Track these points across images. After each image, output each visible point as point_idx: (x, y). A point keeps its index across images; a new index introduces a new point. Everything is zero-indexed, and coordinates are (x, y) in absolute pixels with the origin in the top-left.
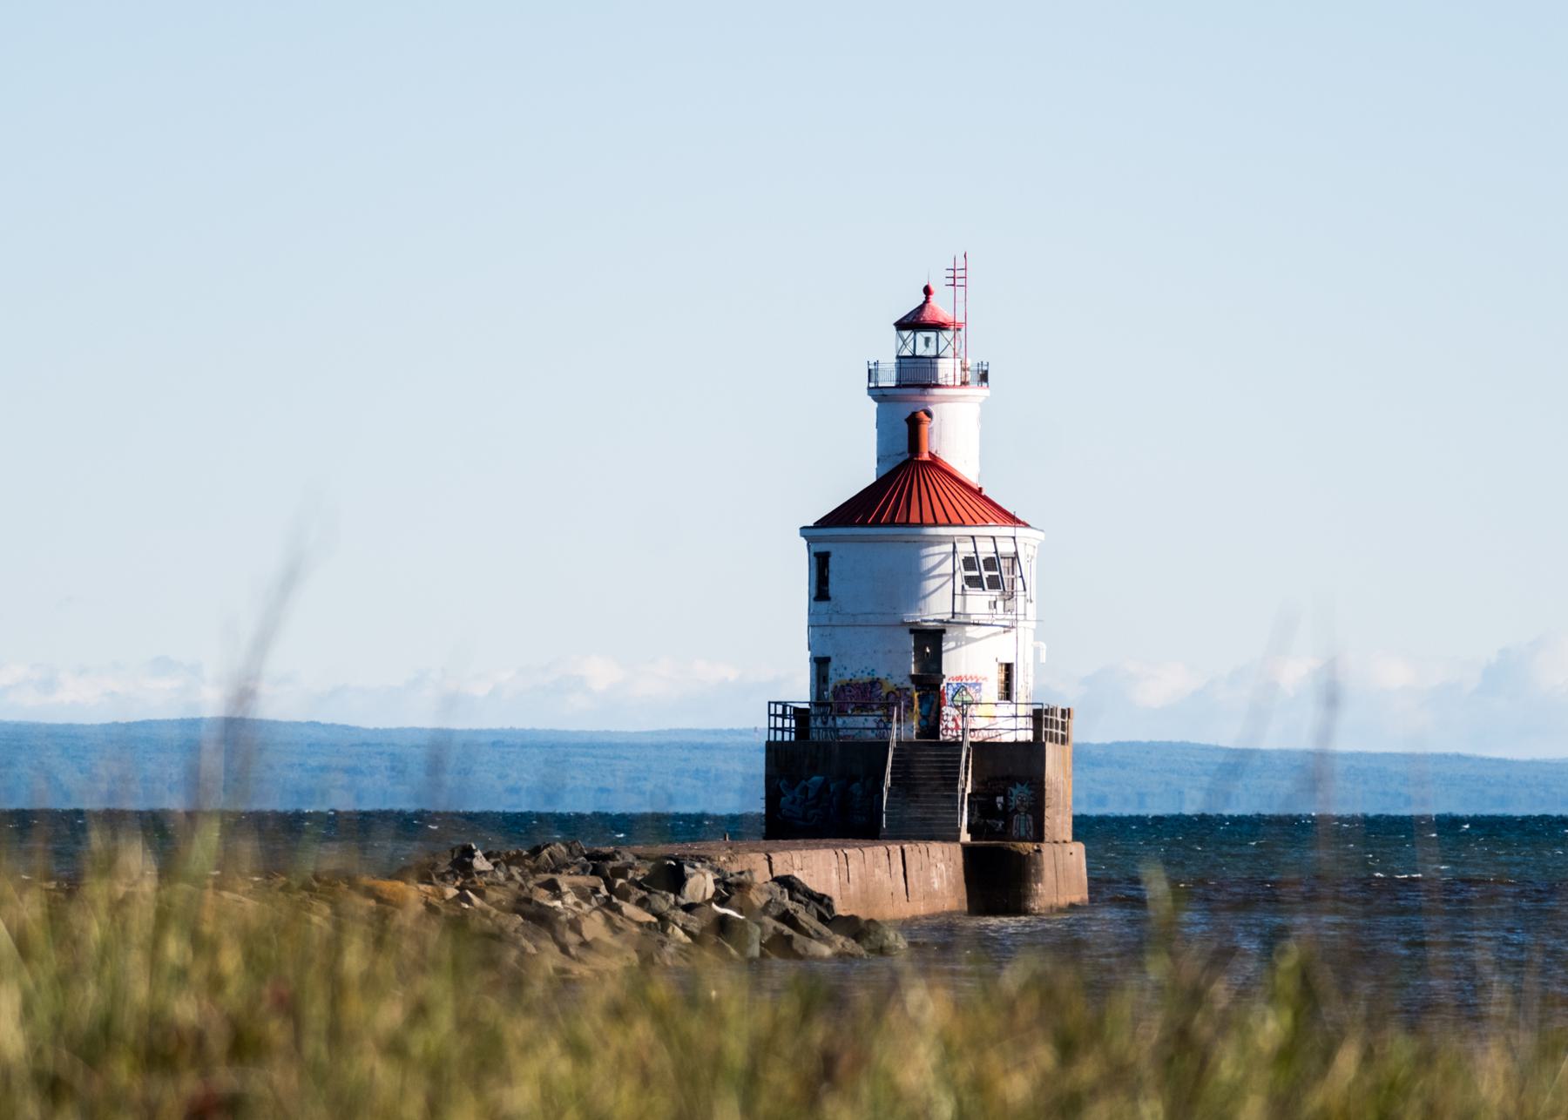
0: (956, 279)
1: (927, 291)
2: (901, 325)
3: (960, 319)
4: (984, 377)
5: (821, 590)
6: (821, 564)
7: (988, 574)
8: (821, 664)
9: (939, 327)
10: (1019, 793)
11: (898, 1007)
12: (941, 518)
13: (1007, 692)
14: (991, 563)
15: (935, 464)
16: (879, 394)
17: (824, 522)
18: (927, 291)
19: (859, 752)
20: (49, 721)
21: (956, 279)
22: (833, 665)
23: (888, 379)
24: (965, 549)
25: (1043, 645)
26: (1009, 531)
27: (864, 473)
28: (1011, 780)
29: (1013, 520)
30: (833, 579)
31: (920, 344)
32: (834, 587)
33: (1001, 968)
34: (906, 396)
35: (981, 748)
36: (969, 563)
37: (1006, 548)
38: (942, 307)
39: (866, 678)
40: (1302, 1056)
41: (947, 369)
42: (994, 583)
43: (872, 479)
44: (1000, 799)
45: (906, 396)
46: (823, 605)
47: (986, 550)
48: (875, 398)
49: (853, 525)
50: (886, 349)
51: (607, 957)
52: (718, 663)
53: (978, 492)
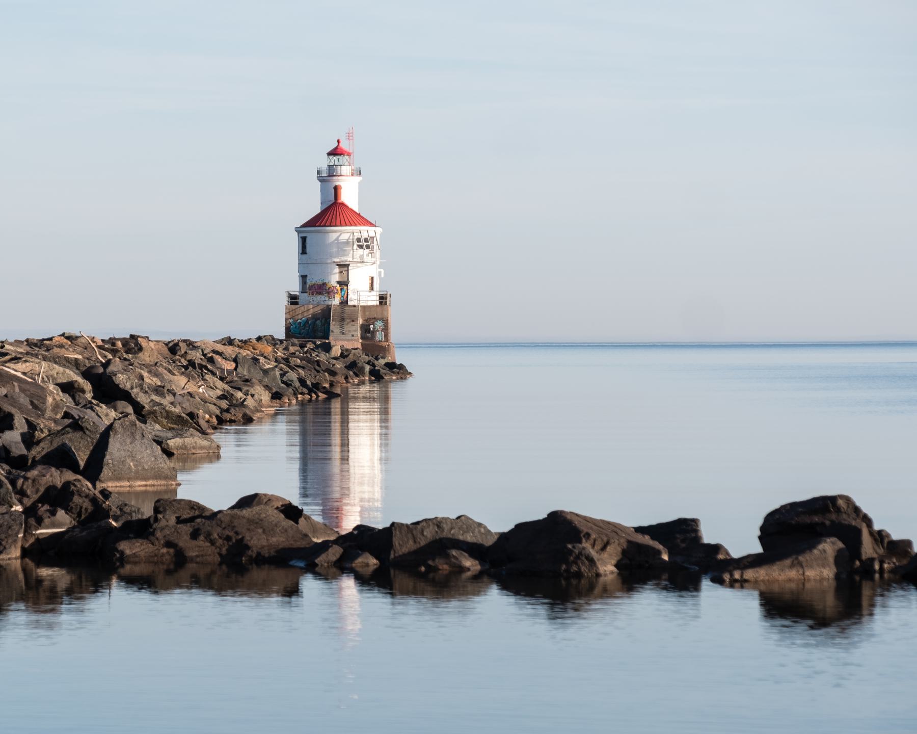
0: (349, 137)
2: (329, 154)
3: (351, 151)
4: (360, 173)
5: (303, 250)
6: (304, 240)
7: (365, 244)
8: (304, 278)
9: (341, 154)
10: (379, 324)
11: (139, 339)
12: (343, 223)
13: (372, 288)
14: (366, 240)
15: (343, 204)
17: (304, 226)
18: (338, 141)
21: (349, 137)
22: (308, 278)
23: (325, 174)
24: (357, 235)
25: (382, 271)
26: (373, 228)
27: (317, 210)
28: (376, 319)
29: (372, 225)
30: (308, 246)
32: (308, 250)
34: (327, 177)
35: (364, 307)
36: (359, 240)
37: (372, 234)
38: (344, 145)
39: (321, 282)
42: (368, 247)
43: (319, 211)
44: (372, 326)
45: (327, 177)
46: (304, 256)
47: (365, 235)
48: (320, 181)
49: (315, 226)
51: (381, 435)
53: (359, 214)
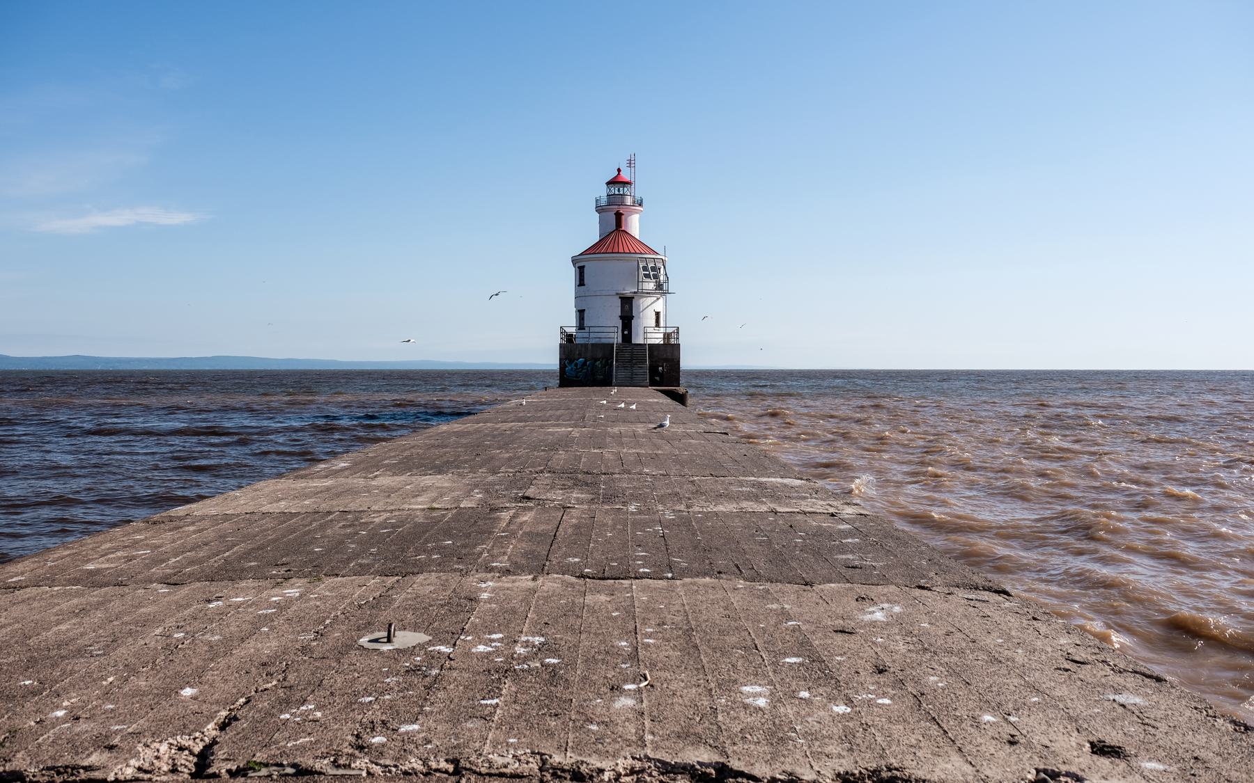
0: (630, 163)
1: (619, 170)
2: (608, 183)
5: (581, 282)
6: (581, 271)
16: (600, 209)
18: (619, 170)
19: (611, 359)
20: (233, 368)
21: (630, 163)
23: (604, 201)
31: (614, 190)
33: (653, 383)
34: (614, 213)
38: (625, 175)
40: (1251, 704)
41: (629, 201)
43: (597, 239)
45: (614, 213)
50: (602, 192)
52: (531, 327)
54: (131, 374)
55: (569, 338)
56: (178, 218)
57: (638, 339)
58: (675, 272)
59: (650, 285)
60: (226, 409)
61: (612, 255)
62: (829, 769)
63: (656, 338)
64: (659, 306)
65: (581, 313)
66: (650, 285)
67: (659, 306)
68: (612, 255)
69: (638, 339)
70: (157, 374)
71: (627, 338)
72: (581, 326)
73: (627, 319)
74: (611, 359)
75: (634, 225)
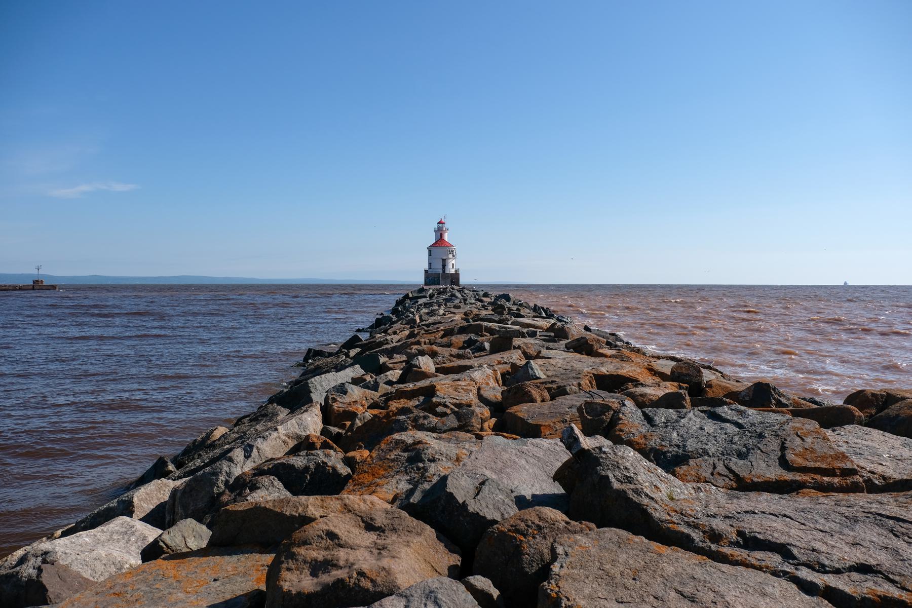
5: (430, 254)
6: (430, 252)
34: (440, 232)
38: (443, 221)
45: (440, 232)
50: (436, 226)
54: (265, 286)
55: (426, 271)
56: (119, 187)
57: (447, 272)
58: (458, 251)
59: (451, 256)
60: (13, 384)
61: (440, 246)
62: (205, 604)
63: (453, 271)
64: (454, 262)
65: (430, 264)
66: (451, 256)
67: (454, 262)
68: (440, 246)
69: (447, 272)
70: (283, 285)
71: (444, 271)
72: (430, 268)
73: (444, 266)
74: (440, 279)
75: (446, 237)
